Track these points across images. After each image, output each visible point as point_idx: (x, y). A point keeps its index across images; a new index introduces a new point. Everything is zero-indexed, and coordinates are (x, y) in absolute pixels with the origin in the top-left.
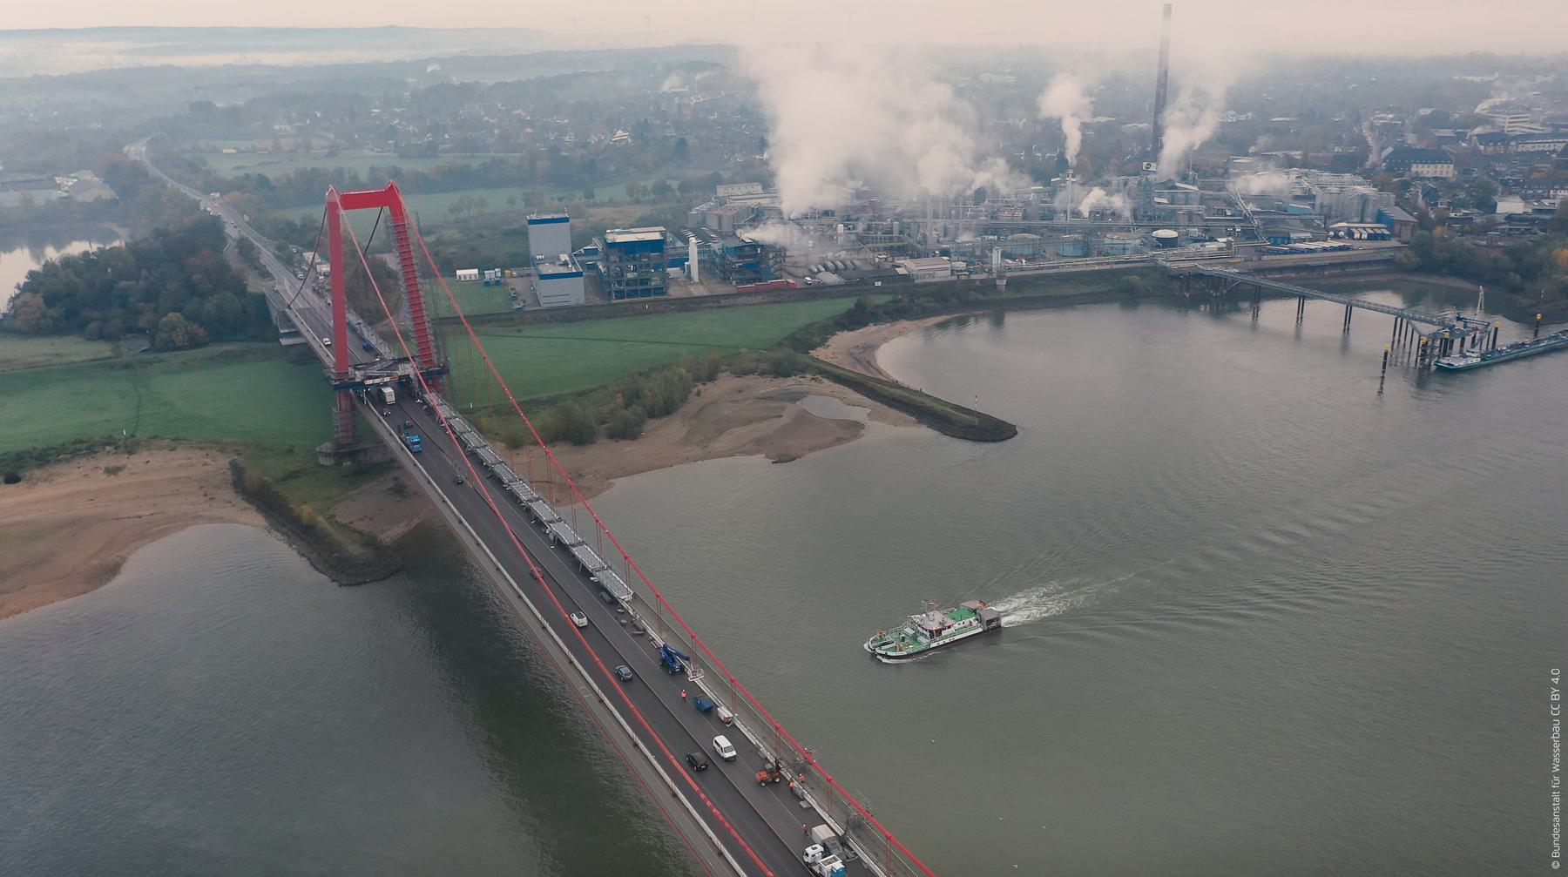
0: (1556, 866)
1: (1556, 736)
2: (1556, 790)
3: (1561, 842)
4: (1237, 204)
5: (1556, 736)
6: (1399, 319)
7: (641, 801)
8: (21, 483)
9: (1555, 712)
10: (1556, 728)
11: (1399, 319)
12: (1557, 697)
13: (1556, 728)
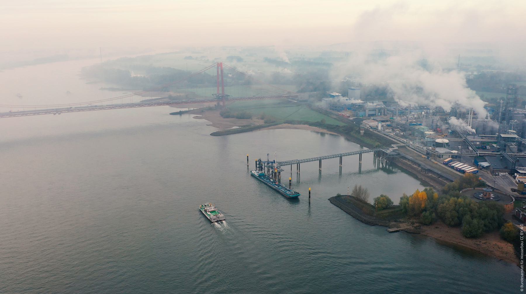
0: (522, 290)
1: (522, 247)
2: (522, 265)
3: (523, 282)
4: (508, 184)
5: (522, 247)
6: (298, 164)
7: (437, 228)
8: (397, 174)
9: (522, 239)
10: (522, 244)
11: (298, 164)
12: (522, 234)
13: (522, 244)
